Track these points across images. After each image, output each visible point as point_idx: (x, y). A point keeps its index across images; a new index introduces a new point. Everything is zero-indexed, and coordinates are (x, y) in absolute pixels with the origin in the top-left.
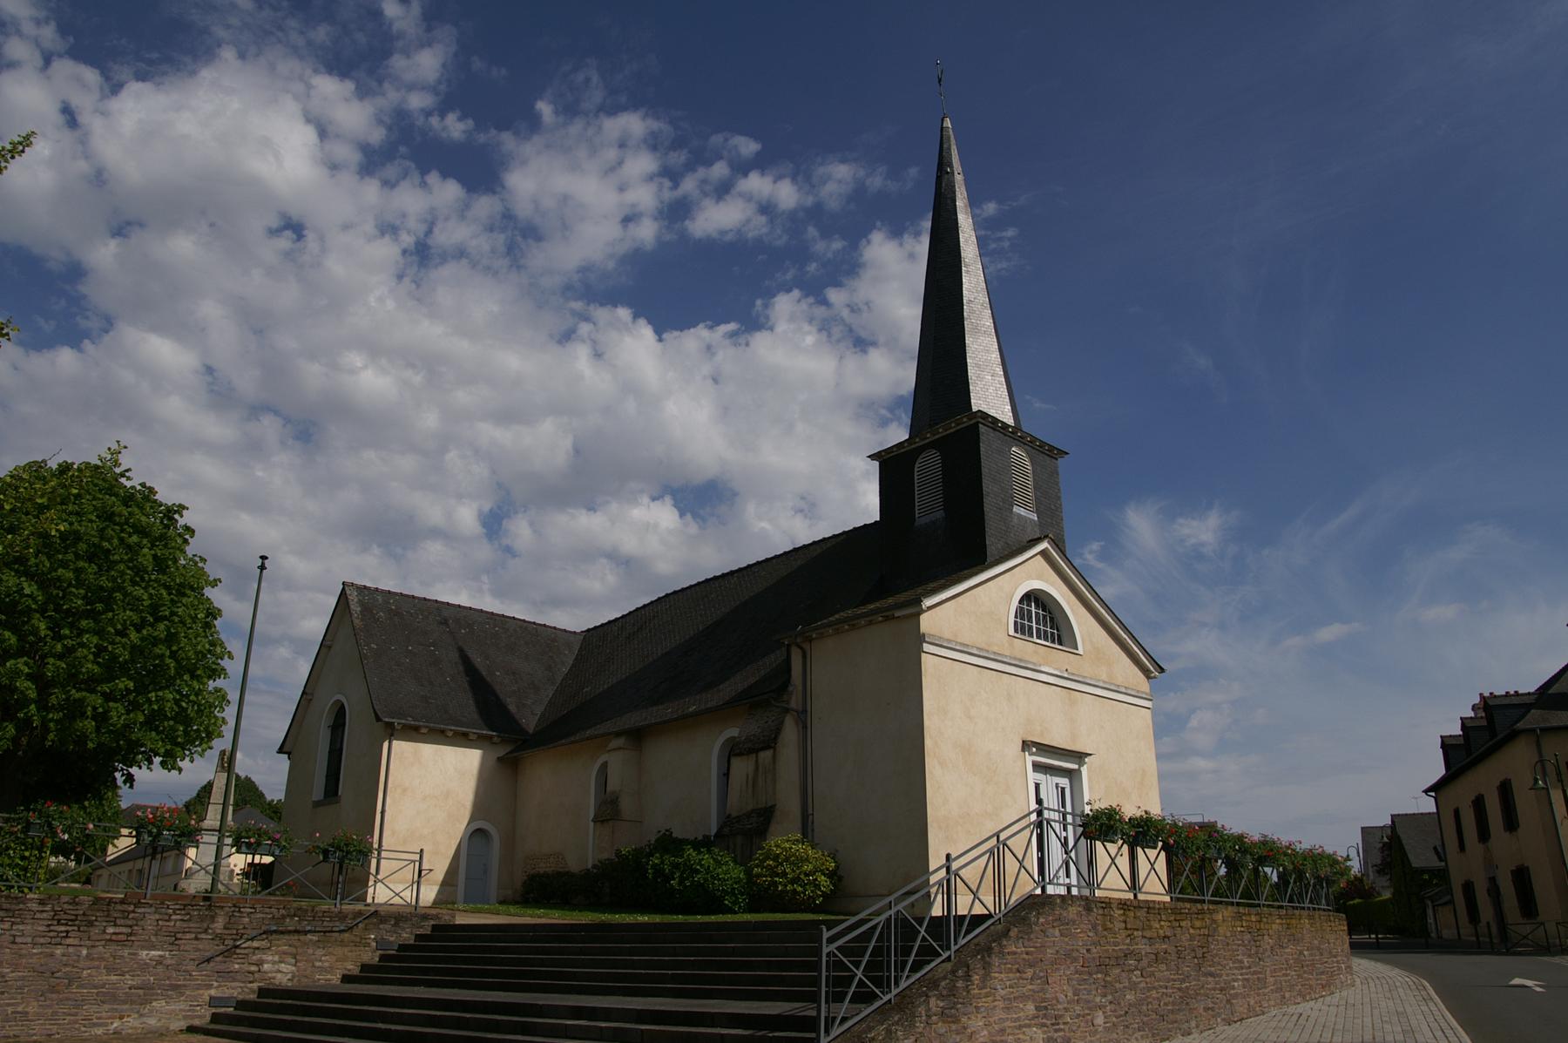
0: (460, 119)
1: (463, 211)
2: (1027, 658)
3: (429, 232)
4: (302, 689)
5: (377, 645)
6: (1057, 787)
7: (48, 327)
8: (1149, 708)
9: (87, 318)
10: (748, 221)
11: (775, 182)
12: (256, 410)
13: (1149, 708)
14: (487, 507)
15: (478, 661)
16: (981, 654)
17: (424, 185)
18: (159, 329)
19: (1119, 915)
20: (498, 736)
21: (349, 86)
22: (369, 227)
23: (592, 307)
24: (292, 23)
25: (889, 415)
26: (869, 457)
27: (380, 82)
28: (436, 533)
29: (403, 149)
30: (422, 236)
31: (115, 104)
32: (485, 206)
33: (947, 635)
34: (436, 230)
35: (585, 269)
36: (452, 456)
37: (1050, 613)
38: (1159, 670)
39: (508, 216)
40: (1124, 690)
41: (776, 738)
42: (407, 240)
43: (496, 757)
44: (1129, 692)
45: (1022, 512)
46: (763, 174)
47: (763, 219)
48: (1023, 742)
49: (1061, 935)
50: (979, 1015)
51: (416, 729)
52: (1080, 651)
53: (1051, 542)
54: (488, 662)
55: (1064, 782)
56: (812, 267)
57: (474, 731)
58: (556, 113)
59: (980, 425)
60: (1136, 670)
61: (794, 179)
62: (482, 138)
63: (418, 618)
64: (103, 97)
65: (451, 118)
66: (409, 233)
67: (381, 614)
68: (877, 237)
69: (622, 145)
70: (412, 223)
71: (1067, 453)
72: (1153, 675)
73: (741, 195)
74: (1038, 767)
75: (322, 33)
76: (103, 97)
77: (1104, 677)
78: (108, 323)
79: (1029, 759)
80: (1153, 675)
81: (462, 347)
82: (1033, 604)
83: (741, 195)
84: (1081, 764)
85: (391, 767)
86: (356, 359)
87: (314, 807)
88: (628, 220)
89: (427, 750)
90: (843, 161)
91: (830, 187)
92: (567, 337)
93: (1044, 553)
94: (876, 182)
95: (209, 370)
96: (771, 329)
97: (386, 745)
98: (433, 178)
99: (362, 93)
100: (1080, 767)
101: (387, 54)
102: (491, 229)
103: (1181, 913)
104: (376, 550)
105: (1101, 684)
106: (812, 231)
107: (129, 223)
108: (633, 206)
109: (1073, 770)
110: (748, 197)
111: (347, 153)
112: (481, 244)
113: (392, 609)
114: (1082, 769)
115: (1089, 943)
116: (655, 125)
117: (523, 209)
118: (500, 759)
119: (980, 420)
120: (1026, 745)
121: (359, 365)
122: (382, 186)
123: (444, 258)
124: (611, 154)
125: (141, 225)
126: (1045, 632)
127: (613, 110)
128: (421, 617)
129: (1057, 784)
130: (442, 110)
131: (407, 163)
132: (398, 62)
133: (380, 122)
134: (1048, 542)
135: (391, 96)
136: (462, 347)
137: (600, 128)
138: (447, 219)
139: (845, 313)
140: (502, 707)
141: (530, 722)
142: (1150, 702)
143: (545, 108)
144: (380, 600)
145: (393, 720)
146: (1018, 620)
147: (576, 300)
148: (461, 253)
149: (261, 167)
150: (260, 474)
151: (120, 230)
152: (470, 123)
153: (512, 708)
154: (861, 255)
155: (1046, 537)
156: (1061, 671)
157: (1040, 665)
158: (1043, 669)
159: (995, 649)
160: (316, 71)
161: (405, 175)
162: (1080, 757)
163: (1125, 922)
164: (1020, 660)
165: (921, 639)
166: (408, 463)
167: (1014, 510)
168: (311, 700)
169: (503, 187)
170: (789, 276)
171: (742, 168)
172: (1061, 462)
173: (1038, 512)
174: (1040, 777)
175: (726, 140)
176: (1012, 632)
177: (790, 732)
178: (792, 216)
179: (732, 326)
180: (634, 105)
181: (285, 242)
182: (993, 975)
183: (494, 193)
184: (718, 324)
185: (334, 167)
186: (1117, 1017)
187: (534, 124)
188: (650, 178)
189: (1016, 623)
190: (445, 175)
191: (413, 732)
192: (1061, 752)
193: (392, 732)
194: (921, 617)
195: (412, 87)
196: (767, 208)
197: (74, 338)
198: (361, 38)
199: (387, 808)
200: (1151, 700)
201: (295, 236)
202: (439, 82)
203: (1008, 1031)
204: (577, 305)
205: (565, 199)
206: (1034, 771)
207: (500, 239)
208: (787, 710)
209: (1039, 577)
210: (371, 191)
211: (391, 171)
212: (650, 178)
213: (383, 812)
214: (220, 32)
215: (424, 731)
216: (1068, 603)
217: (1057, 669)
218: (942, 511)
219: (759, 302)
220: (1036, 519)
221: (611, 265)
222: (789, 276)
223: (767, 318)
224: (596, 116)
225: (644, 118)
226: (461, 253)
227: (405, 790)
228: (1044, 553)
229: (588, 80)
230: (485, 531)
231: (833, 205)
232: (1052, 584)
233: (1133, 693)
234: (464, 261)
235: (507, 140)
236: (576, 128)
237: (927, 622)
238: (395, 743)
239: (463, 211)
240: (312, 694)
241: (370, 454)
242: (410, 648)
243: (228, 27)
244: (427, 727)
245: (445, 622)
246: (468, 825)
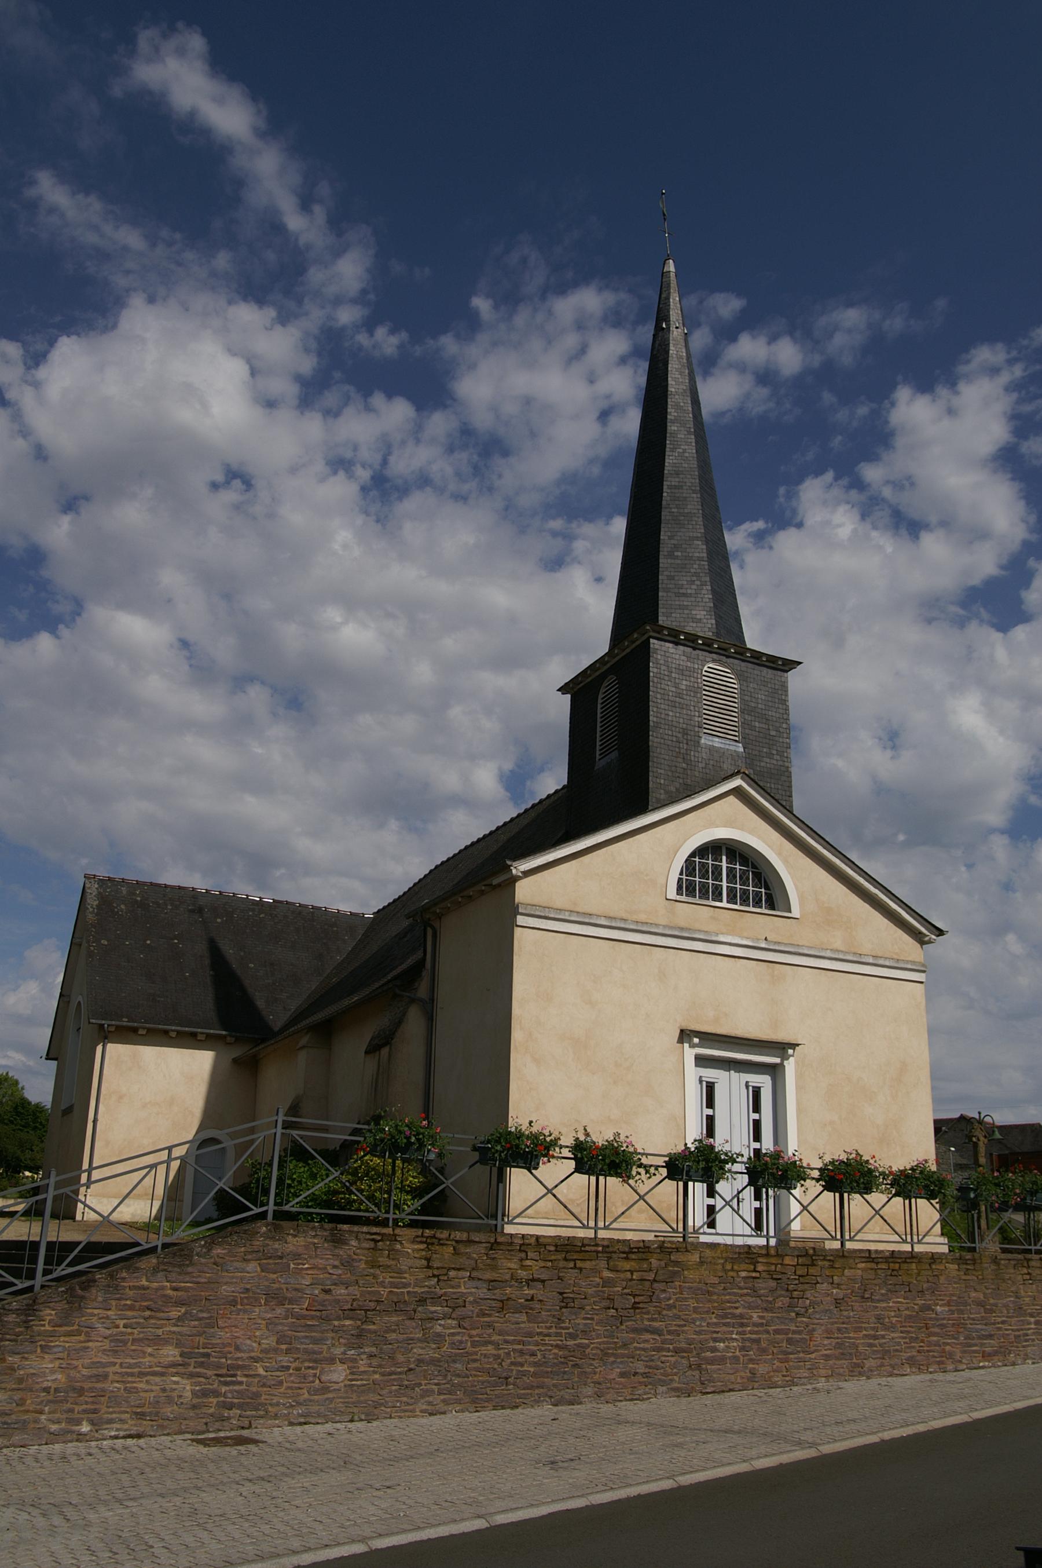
0: (392, 332)
1: (416, 433)
2: (697, 926)
3: (385, 462)
4: (59, 991)
5: (108, 941)
6: (747, 1087)
7: (22, 616)
8: (922, 982)
9: (57, 602)
10: (747, 396)
11: (769, 343)
12: (241, 682)
13: (922, 982)
14: (509, 766)
15: (229, 951)
16: (614, 924)
17: (369, 409)
18: (128, 605)
19: (413, 1250)
20: (231, 1036)
21: (271, 313)
22: (320, 466)
23: (574, 525)
24: (189, 255)
25: (961, 612)
26: (558, 690)
27: (300, 302)
28: (458, 801)
29: (337, 375)
30: (378, 467)
31: (42, 373)
32: (440, 423)
33: (559, 904)
34: (392, 459)
35: (568, 478)
36: (456, 712)
37: (754, 866)
38: (937, 933)
39: (466, 432)
40: (871, 961)
41: (394, 1033)
42: (364, 475)
43: (230, 1060)
44: (881, 962)
45: (717, 742)
46: (754, 337)
47: (764, 392)
48: (682, 1031)
49: (262, 1271)
50: (46, 1356)
51: (135, 1030)
52: (796, 912)
53: (747, 778)
54: (242, 954)
55: (764, 1081)
56: (837, 441)
57: (173, 1028)
58: (496, 307)
59: (652, 641)
60: (900, 933)
61: (791, 333)
62: (418, 351)
63: (166, 909)
64: (29, 368)
65: (381, 332)
66: (363, 466)
67: (123, 907)
68: (903, 394)
69: (580, 326)
70: (365, 454)
71: (801, 663)
72: (927, 939)
73: (731, 366)
74: (701, 1061)
75: (222, 260)
76: (29, 368)
77: (838, 944)
78: (78, 607)
79: (689, 1053)
80: (927, 939)
81: (442, 589)
82: (724, 858)
83: (731, 366)
84: (785, 1057)
85: (105, 1072)
86: (333, 614)
87: (63, 1116)
88: (604, 416)
89: (149, 1053)
90: (850, 304)
91: (839, 340)
92: (556, 563)
93: (737, 792)
94: (896, 324)
95: (184, 644)
96: (800, 525)
97: (99, 1048)
98: (378, 399)
99: (284, 319)
100: (782, 1061)
101: (301, 270)
102: (450, 449)
103: (581, 1251)
104: (393, 824)
105: (828, 954)
106: (828, 398)
107: (76, 498)
108: (608, 397)
109: (777, 1064)
110: (741, 367)
111: (284, 387)
112: (442, 467)
113: (137, 901)
114: (786, 1063)
115: (329, 1282)
116: (610, 298)
117: (482, 420)
118: (235, 1061)
119: (652, 634)
120: (685, 1035)
121: (339, 619)
122: (324, 416)
123: (403, 491)
124: (571, 341)
125: (87, 498)
126: (745, 893)
127: (563, 289)
128: (169, 907)
129: (747, 1082)
130: (369, 325)
131: (347, 387)
132: (315, 275)
133: (307, 350)
134: (742, 778)
135: (315, 317)
136: (442, 589)
137: (550, 313)
138: (403, 443)
139: (887, 492)
140: (247, 1002)
141: (277, 1017)
142: (923, 975)
143: (482, 304)
144: (124, 892)
145: (103, 1022)
146: (684, 877)
147: (554, 518)
148: (424, 481)
149: (185, 415)
150: (259, 751)
151: (70, 505)
152: (404, 335)
153: (260, 1003)
154: (887, 422)
155: (738, 773)
156: (753, 940)
157: (717, 934)
158: (722, 938)
159: (642, 917)
160: (230, 303)
161: (347, 400)
162: (782, 1048)
163: (428, 1260)
164: (682, 929)
165: (514, 910)
166: (408, 724)
167: (703, 741)
168: (69, 1002)
169: (455, 400)
170: (810, 456)
171: (728, 333)
172: (793, 677)
173: (746, 741)
174: (710, 1074)
175: (701, 302)
176: (672, 893)
177: (414, 1022)
178: (798, 381)
179: (760, 525)
180: (583, 278)
181: (230, 496)
182: (88, 1311)
183: (445, 407)
184: (740, 523)
185: (270, 404)
186: (383, 1374)
187: (472, 324)
188: (623, 360)
189: (680, 880)
190: (390, 395)
191: (129, 1034)
192: (746, 1042)
193: (105, 1036)
194: (517, 884)
195: (338, 301)
196: (766, 376)
197: (51, 624)
198: (271, 256)
199: (99, 1117)
200: (924, 972)
201: (244, 487)
202: (364, 292)
203: (111, 1377)
204: (557, 524)
205: (528, 401)
206: (696, 1066)
207: (462, 457)
208: (413, 1001)
209: (729, 824)
210: (313, 426)
211: (330, 398)
212: (623, 360)
213: (95, 1121)
214: (121, 281)
215: (141, 1032)
216: (779, 854)
217: (742, 937)
218: (616, 751)
219: (782, 490)
220: (741, 750)
221: (596, 470)
222: (810, 456)
223: (794, 512)
224: (543, 297)
225: (600, 290)
226: (424, 481)
227: (121, 1097)
228: (737, 792)
229: (524, 260)
230: (508, 794)
231: (847, 360)
232: (751, 832)
233: (887, 963)
234: (428, 489)
235: (449, 344)
236: (521, 318)
237: (525, 891)
238: (109, 1046)
239: (416, 433)
240: (69, 996)
241: (365, 719)
242: (148, 942)
243: (128, 272)
244: (144, 1028)
245: (200, 910)
246: (197, 1133)
